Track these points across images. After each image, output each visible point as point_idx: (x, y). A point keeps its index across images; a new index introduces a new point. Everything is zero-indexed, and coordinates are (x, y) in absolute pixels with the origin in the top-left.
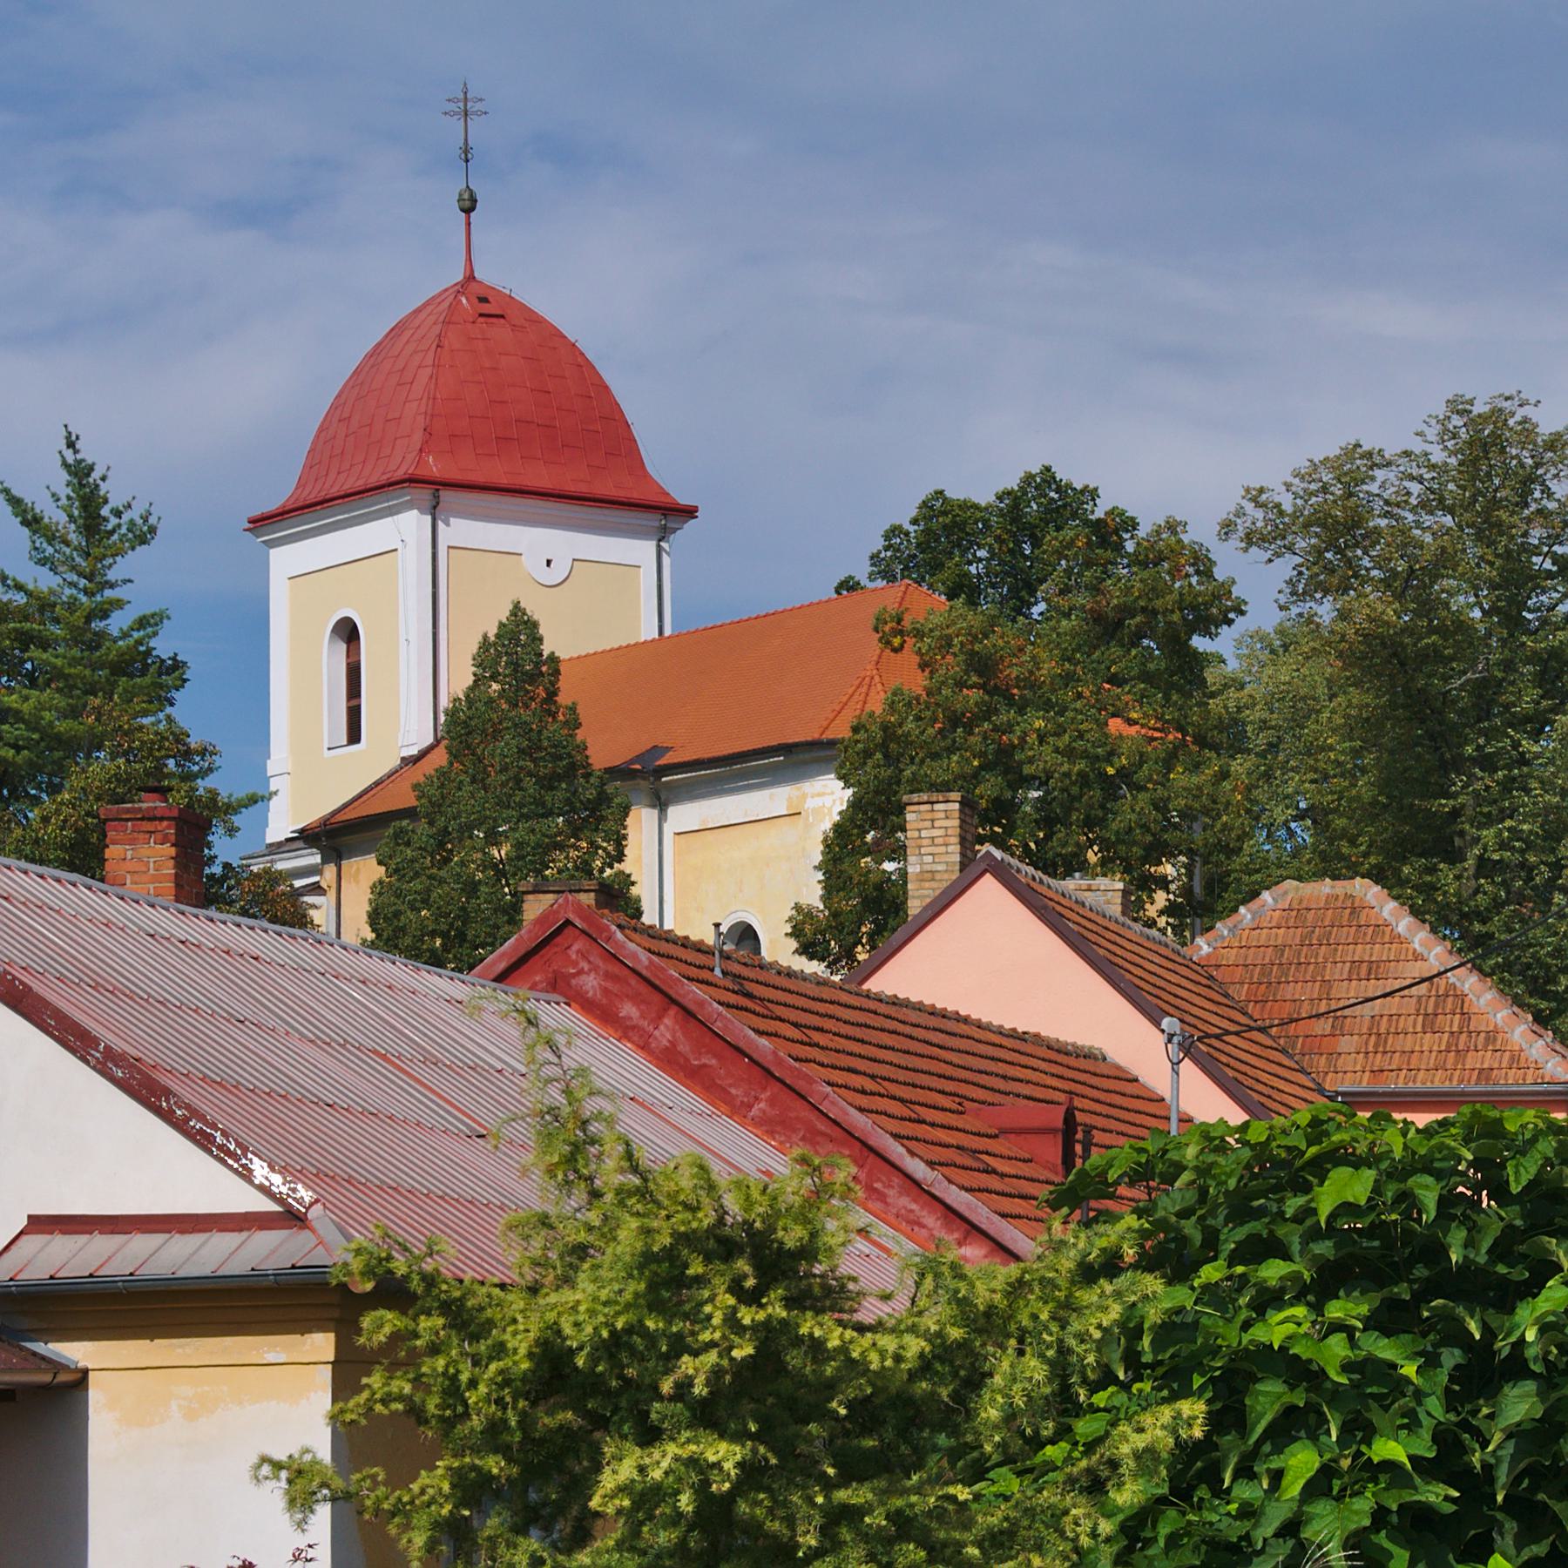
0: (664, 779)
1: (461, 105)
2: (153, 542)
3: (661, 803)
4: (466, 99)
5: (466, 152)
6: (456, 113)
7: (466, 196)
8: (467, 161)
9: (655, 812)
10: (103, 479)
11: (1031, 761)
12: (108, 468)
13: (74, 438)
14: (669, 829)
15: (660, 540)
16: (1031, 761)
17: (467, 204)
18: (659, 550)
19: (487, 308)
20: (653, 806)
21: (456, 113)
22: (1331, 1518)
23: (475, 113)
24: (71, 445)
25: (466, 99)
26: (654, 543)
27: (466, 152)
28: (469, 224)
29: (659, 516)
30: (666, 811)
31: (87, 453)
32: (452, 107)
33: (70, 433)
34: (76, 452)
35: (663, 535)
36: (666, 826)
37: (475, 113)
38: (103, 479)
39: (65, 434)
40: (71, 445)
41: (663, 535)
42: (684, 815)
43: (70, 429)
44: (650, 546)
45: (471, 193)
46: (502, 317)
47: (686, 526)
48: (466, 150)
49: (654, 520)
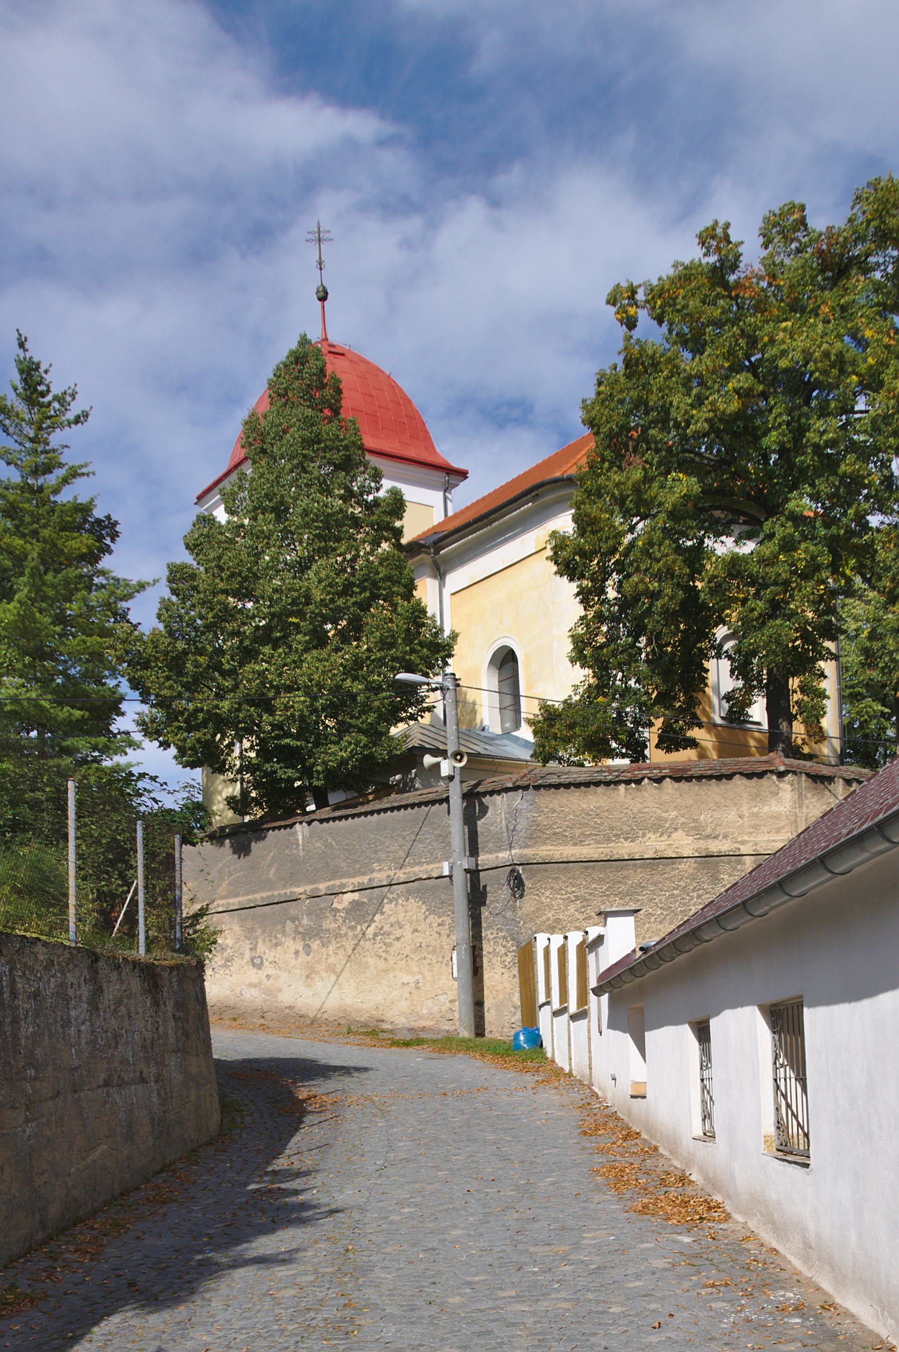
0: (442, 552)
1: (317, 235)
2: (85, 423)
3: (440, 572)
4: (319, 232)
5: (320, 264)
6: (313, 240)
7: (321, 289)
8: (321, 269)
9: (437, 582)
10: (46, 372)
11: (784, 353)
12: (51, 365)
13: (23, 339)
14: (447, 592)
15: (445, 491)
16: (784, 353)
17: (322, 294)
18: (445, 498)
19: (333, 350)
20: (435, 577)
21: (313, 240)
22: (584, 1242)
23: (325, 240)
24: (22, 345)
25: (319, 232)
26: (441, 493)
27: (320, 264)
28: (323, 307)
29: (444, 474)
30: (444, 579)
31: (36, 353)
32: (311, 236)
33: (20, 335)
34: (26, 350)
35: (447, 488)
36: (444, 591)
37: (325, 240)
38: (46, 372)
39: (16, 335)
40: (22, 345)
41: (447, 488)
42: (457, 578)
43: (21, 332)
44: (440, 495)
45: (324, 287)
46: (343, 355)
47: (461, 484)
48: (320, 263)
49: (441, 477)
